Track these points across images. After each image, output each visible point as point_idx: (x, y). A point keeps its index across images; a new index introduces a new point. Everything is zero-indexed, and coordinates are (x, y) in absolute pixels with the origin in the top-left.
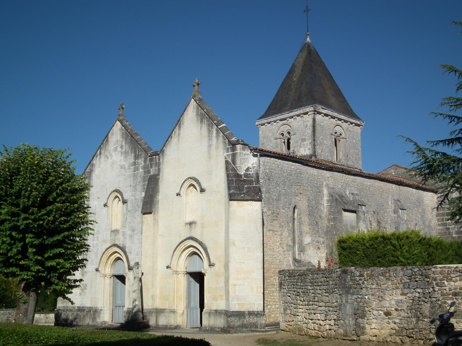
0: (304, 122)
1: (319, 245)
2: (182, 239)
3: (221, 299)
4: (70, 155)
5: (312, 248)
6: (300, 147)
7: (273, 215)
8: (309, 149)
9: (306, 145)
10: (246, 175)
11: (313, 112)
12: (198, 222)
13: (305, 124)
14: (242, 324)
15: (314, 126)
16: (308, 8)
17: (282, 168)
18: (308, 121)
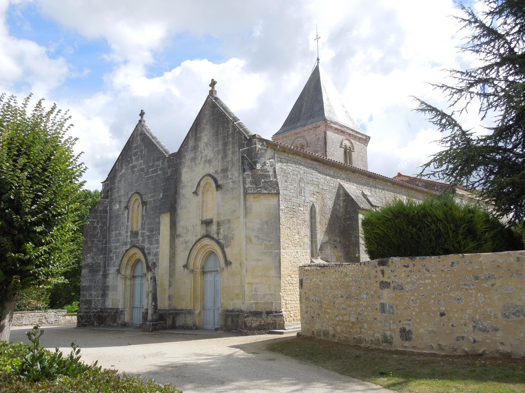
0: (316, 135)
1: (336, 243)
2: (199, 237)
3: (238, 298)
4: (72, 125)
5: (329, 247)
10: (262, 170)
12: (233, 264)
13: (317, 137)
14: (260, 325)
16: (318, 37)
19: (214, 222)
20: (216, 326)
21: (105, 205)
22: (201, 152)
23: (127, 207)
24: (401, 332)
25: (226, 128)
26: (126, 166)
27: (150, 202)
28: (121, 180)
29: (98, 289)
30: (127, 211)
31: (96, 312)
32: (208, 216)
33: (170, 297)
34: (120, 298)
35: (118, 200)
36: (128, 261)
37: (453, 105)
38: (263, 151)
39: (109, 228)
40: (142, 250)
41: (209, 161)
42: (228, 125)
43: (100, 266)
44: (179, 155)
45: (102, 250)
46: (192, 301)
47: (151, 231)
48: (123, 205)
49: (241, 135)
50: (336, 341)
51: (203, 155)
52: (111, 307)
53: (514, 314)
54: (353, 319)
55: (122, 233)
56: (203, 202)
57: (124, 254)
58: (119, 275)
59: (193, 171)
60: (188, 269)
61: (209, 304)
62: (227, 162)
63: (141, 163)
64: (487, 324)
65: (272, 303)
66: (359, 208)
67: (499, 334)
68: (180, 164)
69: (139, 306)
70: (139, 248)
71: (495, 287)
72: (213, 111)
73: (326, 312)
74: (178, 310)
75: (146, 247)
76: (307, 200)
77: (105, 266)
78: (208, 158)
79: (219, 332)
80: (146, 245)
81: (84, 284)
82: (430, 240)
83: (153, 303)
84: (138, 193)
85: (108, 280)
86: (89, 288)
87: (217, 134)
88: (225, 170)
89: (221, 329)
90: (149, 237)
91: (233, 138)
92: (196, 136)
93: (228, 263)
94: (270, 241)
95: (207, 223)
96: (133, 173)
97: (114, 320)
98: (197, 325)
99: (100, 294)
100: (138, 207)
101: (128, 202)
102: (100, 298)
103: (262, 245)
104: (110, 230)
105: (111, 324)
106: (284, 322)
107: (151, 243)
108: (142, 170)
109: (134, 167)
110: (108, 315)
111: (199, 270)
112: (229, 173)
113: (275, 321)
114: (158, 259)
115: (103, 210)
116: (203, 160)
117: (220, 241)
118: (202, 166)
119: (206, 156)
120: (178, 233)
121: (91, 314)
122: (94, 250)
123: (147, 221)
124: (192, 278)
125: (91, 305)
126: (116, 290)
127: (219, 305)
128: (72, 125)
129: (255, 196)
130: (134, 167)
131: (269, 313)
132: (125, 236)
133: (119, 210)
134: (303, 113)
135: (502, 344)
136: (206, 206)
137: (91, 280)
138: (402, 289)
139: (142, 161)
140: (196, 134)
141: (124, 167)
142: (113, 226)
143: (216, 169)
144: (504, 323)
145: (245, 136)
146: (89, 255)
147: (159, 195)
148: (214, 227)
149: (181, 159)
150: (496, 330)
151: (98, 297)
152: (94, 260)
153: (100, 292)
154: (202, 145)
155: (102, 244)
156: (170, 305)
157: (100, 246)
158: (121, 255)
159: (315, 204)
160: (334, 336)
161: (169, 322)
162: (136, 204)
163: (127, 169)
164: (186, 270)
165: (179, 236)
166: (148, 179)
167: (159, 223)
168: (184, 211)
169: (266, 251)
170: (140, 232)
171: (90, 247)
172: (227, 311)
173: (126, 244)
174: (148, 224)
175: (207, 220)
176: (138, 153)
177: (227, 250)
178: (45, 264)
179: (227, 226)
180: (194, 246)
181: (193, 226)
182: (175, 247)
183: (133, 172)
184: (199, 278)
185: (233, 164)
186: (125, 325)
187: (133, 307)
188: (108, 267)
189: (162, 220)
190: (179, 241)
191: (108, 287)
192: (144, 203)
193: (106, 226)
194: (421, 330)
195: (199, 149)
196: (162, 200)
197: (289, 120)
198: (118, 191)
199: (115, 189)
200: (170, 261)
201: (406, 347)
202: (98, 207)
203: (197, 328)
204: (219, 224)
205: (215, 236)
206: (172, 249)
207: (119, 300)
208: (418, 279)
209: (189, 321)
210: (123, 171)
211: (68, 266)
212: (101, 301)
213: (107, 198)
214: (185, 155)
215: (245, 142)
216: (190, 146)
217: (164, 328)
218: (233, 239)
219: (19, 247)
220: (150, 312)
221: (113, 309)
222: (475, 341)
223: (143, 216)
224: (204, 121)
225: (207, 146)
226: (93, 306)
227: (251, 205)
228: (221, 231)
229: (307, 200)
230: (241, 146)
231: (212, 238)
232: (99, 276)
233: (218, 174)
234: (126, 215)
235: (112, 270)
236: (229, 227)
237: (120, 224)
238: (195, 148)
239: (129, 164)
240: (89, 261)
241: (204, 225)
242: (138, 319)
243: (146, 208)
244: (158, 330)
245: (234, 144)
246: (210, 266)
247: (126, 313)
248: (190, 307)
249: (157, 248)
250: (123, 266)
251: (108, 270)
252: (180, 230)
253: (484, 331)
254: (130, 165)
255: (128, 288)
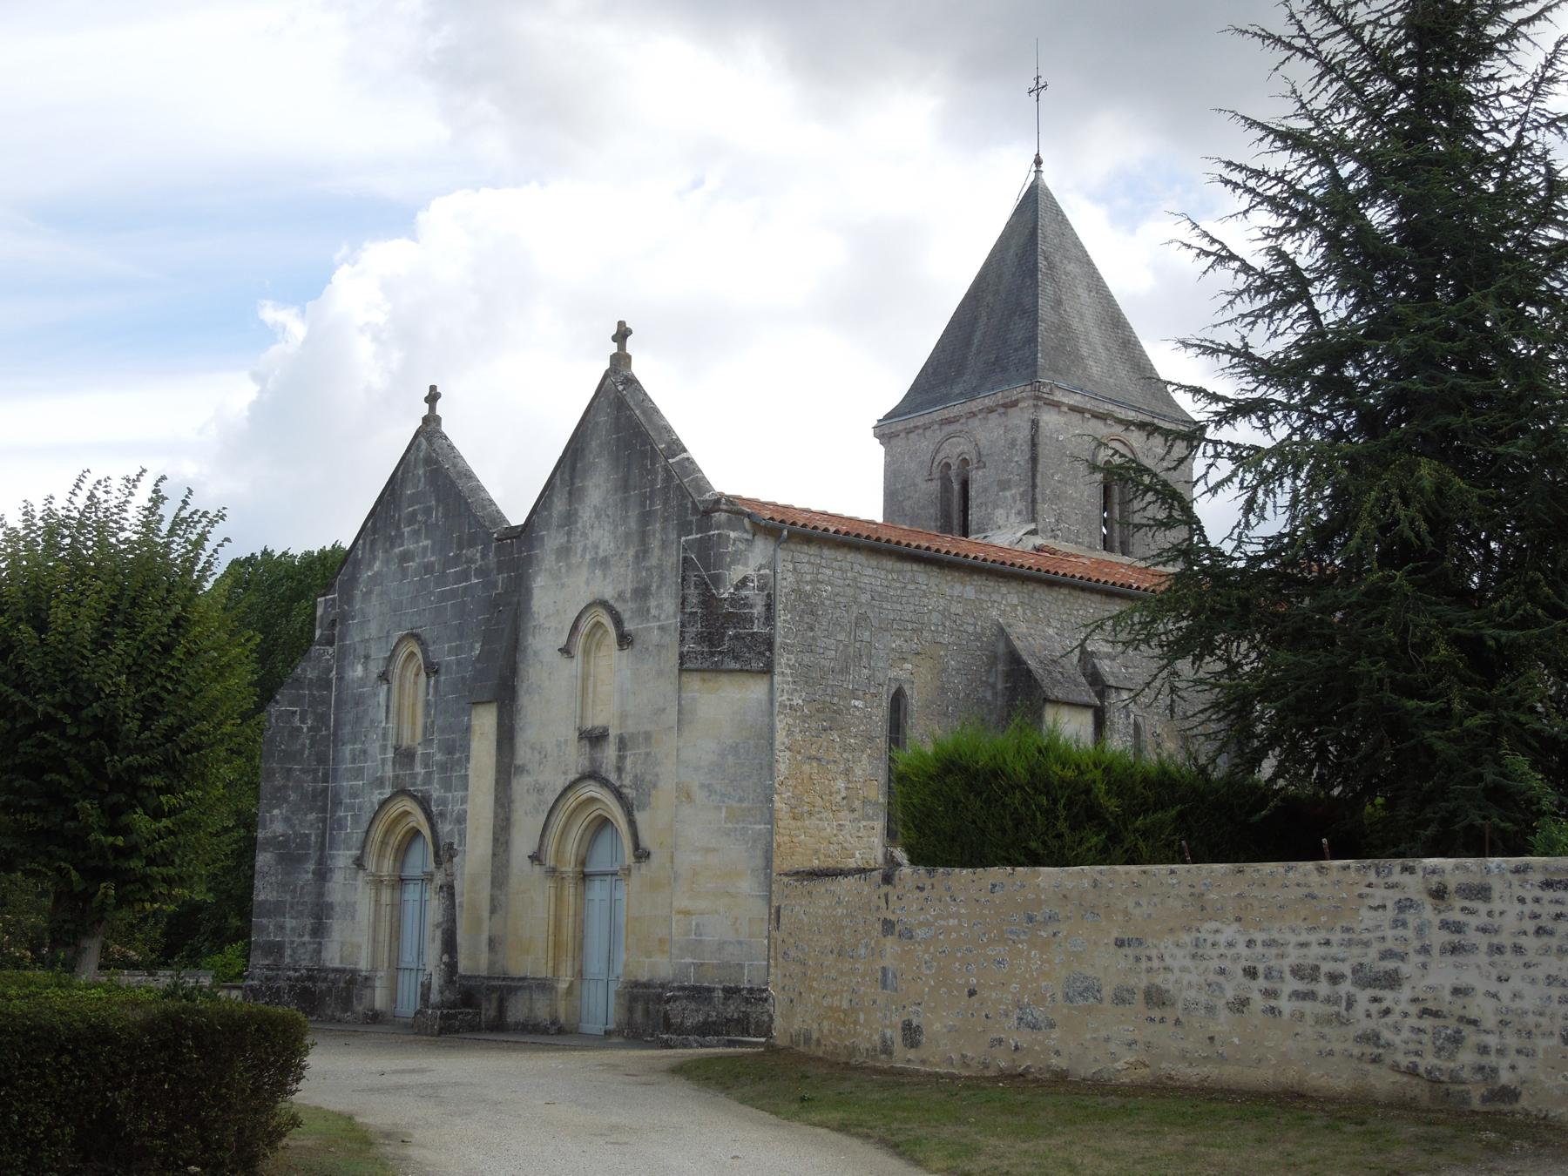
2: (572, 776)
4: (227, 540)
6: (996, 506)
7: (821, 716)
8: (1019, 513)
9: (1010, 501)
10: (734, 601)
11: (1031, 402)
12: (653, 857)
13: (1010, 436)
14: (705, 1023)
15: (1034, 444)
16: (1042, 83)
17: (855, 579)
18: (1017, 427)
19: (611, 738)
20: (611, 1026)
21: (323, 664)
22: (584, 535)
23: (384, 677)
24: (903, 1029)
25: (649, 472)
26: (386, 551)
27: (448, 664)
28: (370, 592)
29: (301, 913)
30: (385, 687)
31: (297, 980)
32: (596, 719)
33: (492, 943)
34: (363, 938)
35: (361, 651)
36: (388, 832)
37: (1175, 468)
38: (742, 546)
39: (335, 734)
40: (424, 803)
41: (604, 563)
42: (653, 464)
43: (309, 846)
44: (526, 533)
45: (314, 797)
46: (551, 954)
47: (449, 749)
48: (375, 669)
49: (684, 497)
50: (820, 1054)
51: (589, 543)
52: (336, 964)
53: (1080, 994)
54: (845, 1005)
55: (370, 751)
56: (585, 677)
57: (376, 814)
58: (361, 873)
59: (563, 585)
60: (541, 864)
61: (595, 965)
62: (648, 569)
63: (425, 548)
64: (1039, 1013)
65: (741, 966)
66: (1047, 700)
67: (1056, 1034)
68: (529, 561)
69: (414, 966)
70: (414, 797)
71: (1057, 939)
72: (617, 418)
73: (811, 989)
74: (513, 979)
75: (435, 795)
76: (880, 676)
77: (323, 844)
78: (601, 554)
79: (615, 1040)
80: (436, 792)
81: (262, 897)
82: (1004, 831)
83: (445, 958)
84: (415, 637)
85: (329, 885)
86: (277, 909)
87: (625, 486)
88: (642, 593)
89: (619, 1032)
90: (444, 767)
91: (666, 502)
92: (572, 484)
93: (641, 855)
94: (741, 800)
95: (594, 738)
96: (405, 576)
97: (346, 1002)
98: (562, 1020)
99: (309, 927)
100: (417, 675)
101: (390, 659)
102: (306, 938)
103: (719, 808)
104: (336, 739)
105: (338, 1014)
106: (771, 1017)
107: (447, 785)
108: (428, 568)
109: (406, 557)
110: (330, 989)
111: (569, 868)
112: (653, 603)
113: (747, 1015)
114: (462, 834)
115: (319, 679)
116: (588, 557)
117: (625, 791)
118: (584, 573)
119: (597, 547)
120: (518, 762)
121: (281, 983)
122: (293, 797)
123: (439, 722)
124: (552, 891)
125: (282, 956)
126: (353, 917)
127: (619, 969)
128: (227, 540)
129: (707, 676)
130: (406, 557)
131: (730, 992)
132: (380, 761)
133: (362, 682)
134: (974, 348)
135: (1057, 1053)
136: (595, 687)
137: (283, 886)
138: (911, 938)
139: (428, 542)
140: (572, 478)
141: (380, 554)
142: (347, 729)
143: (621, 587)
144: (1065, 1011)
145: (693, 502)
146: (276, 812)
147: (472, 648)
148: (610, 752)
149: (531, 547)
150: (1052, 1025)
151: (301, 936)
152: (293, 827)
153: (309, 922)
154: (586, 514)
155: (315, 780)
156: (492, 964)
157: (309, 787)
158: (366, 817)
159: (906, 687)
160: (818, 1043)
161: (488, 1010)
162: (410, 674)
163: (387, 562)
164: (537, 868)
165: (521, 770)
166: (443, 597)
167: (468, 729)
168: (536, 698)
169: (729, 825)
170: (420, 751)
171: (279, 789)
172: (636, 984)
173: (380, 783)
174: (442, 730)
175: (594, 728)
176: (419, 518)
177: (640, 817)
178: (165, 858)
179: (642, 750)
180: (557, 801)
181: (559, 745)
182: (511, 802)
183: (404, 572)
184: (572, 890)
185: (663, 579)
186: (375, 1018)
187: (396, 968)
188: (331, 848)
189: (475, 722)
190: (520, 785)
191: (331, 906)
192: (432, 669)
193: (328, 728)
194: (937, 1026)
195: (579, 525)
196: (479, 666)
197: (930, 370)
198: (362, 624)
199: (353, 618)
200: (496, 840)
201: (909, 1061)
202: (304, 670)
203: (561, 1031)
204: (622, 744)
205: (613, 777)
206: (502, 806)
207: (359, 947)
208: (936, 918)
209: (542, 1010)
210: (377, 566)
211: (214, 862)
212: (310, 947)
213: (331, 644)
214: (542, 538)
215: (694, 519)
216: (555, 513)
217: (474, 1028)
218: (655, 786)
219: (114, 819)
220: (436, 982)
221: (343, 971)
222: (1017, 1048)
223: (427, 704)
224: (593, 444)
225: (598, 517)
226: (287, 960)
227: (694, 699)
228: (628, 762)
229: (880, 676)
230: (684, 528)
231: (605, 783)
232: (307, 875)
233: (625, 601)
234: (382, 698)
235: (342, 858)
236: (648, 754)
237: (366, 724)
238: (569, 519)
239: (392, 546)
240: (278, 828)
241: (585, 742)
242: (408, 1004)
243: (437, 682)
244: (457, 1032)
245: (666, 519)
246: (601, 860)
247: (378, 983)
248: (544, 971)
249: (464, 800)
250: (373, 849)
251: (332, 857)
252: (523, 754)
253: (1034, 1027)
254: (397, 550)
255: (386, 912)
